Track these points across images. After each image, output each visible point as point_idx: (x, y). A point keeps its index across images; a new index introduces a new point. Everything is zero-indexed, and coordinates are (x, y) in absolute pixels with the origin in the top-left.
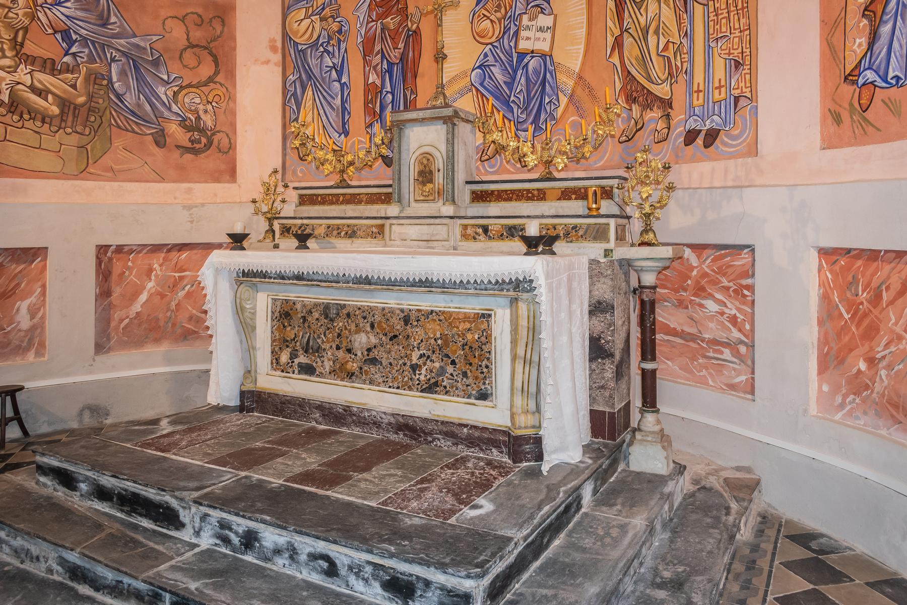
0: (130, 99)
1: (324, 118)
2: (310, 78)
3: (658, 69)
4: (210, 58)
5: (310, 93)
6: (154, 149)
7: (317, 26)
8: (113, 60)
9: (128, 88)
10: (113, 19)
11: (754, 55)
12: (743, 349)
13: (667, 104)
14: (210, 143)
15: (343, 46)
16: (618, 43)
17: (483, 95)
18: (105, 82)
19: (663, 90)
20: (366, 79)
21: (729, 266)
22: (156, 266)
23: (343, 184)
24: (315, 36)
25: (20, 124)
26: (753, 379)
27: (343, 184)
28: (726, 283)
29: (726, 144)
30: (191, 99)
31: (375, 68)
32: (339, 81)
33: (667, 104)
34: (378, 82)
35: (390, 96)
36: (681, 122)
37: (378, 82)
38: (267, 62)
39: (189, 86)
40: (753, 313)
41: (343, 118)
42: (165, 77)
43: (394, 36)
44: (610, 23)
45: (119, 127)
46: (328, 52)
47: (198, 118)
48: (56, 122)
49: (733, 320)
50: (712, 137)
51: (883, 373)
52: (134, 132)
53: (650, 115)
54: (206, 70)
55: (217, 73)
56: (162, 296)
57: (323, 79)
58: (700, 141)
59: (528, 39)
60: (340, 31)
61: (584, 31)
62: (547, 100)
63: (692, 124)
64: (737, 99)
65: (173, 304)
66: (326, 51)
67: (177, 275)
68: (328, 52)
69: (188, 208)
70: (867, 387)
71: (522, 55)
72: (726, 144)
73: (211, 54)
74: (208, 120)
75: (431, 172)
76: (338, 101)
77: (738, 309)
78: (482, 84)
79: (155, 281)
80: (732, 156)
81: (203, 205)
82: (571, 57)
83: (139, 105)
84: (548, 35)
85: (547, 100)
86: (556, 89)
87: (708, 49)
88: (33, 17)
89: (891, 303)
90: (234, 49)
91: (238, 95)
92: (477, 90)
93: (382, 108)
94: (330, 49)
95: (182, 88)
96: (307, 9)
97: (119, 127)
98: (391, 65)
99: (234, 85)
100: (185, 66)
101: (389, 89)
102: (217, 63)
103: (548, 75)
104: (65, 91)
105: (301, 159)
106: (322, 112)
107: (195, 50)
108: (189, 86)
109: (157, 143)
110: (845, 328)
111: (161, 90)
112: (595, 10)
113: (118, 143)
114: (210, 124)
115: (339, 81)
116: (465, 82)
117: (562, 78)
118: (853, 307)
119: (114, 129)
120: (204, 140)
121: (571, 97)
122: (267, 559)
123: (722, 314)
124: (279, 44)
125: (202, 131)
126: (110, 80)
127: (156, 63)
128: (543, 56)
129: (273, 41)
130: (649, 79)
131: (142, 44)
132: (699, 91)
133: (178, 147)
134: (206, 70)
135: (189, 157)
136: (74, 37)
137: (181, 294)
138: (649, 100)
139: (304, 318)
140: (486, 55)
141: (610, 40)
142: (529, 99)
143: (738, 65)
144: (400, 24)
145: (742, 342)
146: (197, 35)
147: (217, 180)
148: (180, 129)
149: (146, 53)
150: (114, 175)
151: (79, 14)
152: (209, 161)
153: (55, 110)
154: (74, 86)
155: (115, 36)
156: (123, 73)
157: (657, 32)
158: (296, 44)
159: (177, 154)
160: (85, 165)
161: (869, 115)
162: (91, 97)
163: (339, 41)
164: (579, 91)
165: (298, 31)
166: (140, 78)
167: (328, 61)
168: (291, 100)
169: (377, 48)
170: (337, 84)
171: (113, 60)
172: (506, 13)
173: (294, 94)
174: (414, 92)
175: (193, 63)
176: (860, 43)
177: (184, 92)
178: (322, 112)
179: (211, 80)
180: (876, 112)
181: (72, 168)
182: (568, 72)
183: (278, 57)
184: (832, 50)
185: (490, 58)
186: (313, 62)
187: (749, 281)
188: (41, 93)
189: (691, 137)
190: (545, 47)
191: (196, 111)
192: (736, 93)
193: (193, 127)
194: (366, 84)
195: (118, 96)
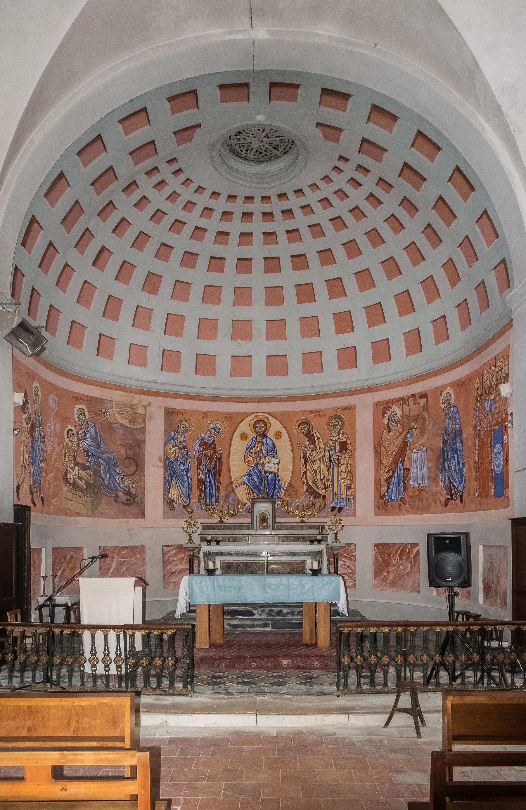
0: (106, 482)
1: (180, 492)
2: (174, 474)
3: (320, 485)
4: (134, 463)
5: (175, 480)
6: (114, 504)
7: (178, 451)
8: (102, 464)
9: (106, 476)
10: (102, 446)
11: (354, 486)
12: (351, 575)
13: (324, 497)
14: (134, 500)
15: (188, 461)
16: (305, 473)
17: (249, 486)
18: (99, 474)
19: (322, 492)
20: (198, 475)
21: (349, 550)
22: (115, 556)
23: (221, 522)
24: (177, 456)
25: (75, 493)
26: (355, 584)
27: (221, 522)
28: (346, 555)
29: (345, 512)
30: (128, 481)
31: (202, 471)
32: (187, 476)
33: (324, 497)
34: (204, 478)
35: (208, 484)
36: (330, 504)
37: (204, 478)
38: (158, 466)
39: (127, 475)
40: (411, 544)
41: (189, 492)
42: (118, 471)
43: (211, 458)
44: (302, 466)
45: (103, 494)
46: (182, 463)
47: (130, 490)
48: (85, 491)
49: (348, 566)
50: (340, 510)
51: (391, 575)
52: (108, 496)
53: (317, 500)
54: (133, 469)
55: (137, 470)
56: (118, 569)
57: (180, 475)
58: (336, 510)
59: (268, 466)
60: (187, 454)
61: (291, 467)
62: (276, 491)
63: (333, 505)
64: (349, 499)
65: (122, 573)
66: (181, 462)
67: (123, 560)
68: (182, 463)
69: (129, 530)
70: (387, 579)
71: (266, 472)
72: (345, 512)
73: (135, 461)
74: (133, 491)
75: (265, 519)
76: (186, 485)
77: (350, 563)
78: (248, 482)
79: (116, 563)
80: (348, 516)
81: (134, 528)
82: (286, 476)
83: (110, 484)
84: (277, 466)
85: (276, 491)
86: (280, 487)
87: (339, 482)
88: (78, 445)
89: (393, 557)
90: (144, 459)
91: (146, 480)
92: (247, 484)
93: (205, 488)
94: (183, 462)
95: (124, 476)
96: (173, 444)
97: (103, 494)
98: (209, 471)
99: (144, 476)
100: (125, 467)
101: (208, 481)
102: (136, 465)
103: (277, 481)
104: (87, 478)
105: (171, 509)
106: (179, 489)
107: (129, 459)
108: (127, 475)
109: (115, 501)
110: (381, 565)
111: (117, 477)
112: (296, 460)
113: (103, 501)
114: (134, 492)
115: (187, 476)
116: (241, 481)
117: (282, 483)
118: (383, 559)
119: (102, 495)
120: (132, 500)
121: (286, 491)
122: (285, 616)
123: (345, 565)
124: (162, 458)
125: (131, 496)
126: (101, 474)
127: (115, 465)
128: (275, 474)
129: (160, 457)
130: (317, 487)
131: (111, 457)
132: (336, 494)
133: (123, 503)
134: (133, 469)
135: (126, 507)
136: (90, 454)
137: (124, 568)
138: (317, 495)
139: (237, 568)
140: (250, 471)
141: (302, 472)
142: (269, 490)
143: (349, 488)
144: (213, 454)
145: (351, 573)
146: (130, 452)
147: (136, 518)
148: (123, 495)
149: (112, 461)
150: (102, 515)
151: (92, 443)
152: (134, 509)
153: (85, 486)
154: (90, 476)
155: (102, 453)
156: (105, 470)
157: (320, 472)
158: (169, 459)
159: (122, 506)
160: (94, 511)
161: (387, 508)
162: (95, 481)
163: (187, 458)
164: (289, 488)
165: (169, 453)
166: (110, 473)
167: (182, 467)
168: (167, 483)
169: (203, 463)
170: (186, 477)
171: (102, 464)
172: (259, 455)
173: (168, 481)
174: (219, 482)
175: (128, 465)
176: (384, 489)
177: (125, 478)
178: (179, 489)
179: (134, 473)
180: (389, 507)
181: (90, 513)
182: (285, 482)
183: (162, 464)
184: (377, 489)
185: (252, 472)
186: (176, 467)
187: (354, 554)
188: (80, 479)
189: (333, 509)
190: (275, 470)
191: (129, 487)
192: (348, 497)
193: (128, 494)
194: (199, 479)
195: (103, 480)
